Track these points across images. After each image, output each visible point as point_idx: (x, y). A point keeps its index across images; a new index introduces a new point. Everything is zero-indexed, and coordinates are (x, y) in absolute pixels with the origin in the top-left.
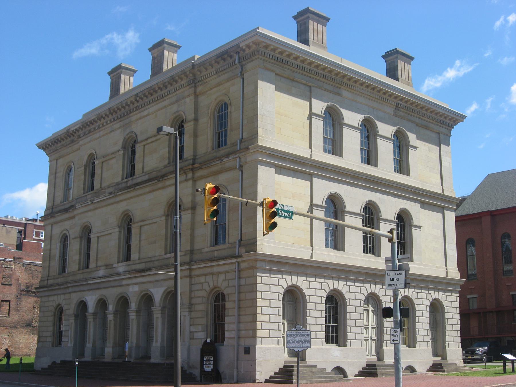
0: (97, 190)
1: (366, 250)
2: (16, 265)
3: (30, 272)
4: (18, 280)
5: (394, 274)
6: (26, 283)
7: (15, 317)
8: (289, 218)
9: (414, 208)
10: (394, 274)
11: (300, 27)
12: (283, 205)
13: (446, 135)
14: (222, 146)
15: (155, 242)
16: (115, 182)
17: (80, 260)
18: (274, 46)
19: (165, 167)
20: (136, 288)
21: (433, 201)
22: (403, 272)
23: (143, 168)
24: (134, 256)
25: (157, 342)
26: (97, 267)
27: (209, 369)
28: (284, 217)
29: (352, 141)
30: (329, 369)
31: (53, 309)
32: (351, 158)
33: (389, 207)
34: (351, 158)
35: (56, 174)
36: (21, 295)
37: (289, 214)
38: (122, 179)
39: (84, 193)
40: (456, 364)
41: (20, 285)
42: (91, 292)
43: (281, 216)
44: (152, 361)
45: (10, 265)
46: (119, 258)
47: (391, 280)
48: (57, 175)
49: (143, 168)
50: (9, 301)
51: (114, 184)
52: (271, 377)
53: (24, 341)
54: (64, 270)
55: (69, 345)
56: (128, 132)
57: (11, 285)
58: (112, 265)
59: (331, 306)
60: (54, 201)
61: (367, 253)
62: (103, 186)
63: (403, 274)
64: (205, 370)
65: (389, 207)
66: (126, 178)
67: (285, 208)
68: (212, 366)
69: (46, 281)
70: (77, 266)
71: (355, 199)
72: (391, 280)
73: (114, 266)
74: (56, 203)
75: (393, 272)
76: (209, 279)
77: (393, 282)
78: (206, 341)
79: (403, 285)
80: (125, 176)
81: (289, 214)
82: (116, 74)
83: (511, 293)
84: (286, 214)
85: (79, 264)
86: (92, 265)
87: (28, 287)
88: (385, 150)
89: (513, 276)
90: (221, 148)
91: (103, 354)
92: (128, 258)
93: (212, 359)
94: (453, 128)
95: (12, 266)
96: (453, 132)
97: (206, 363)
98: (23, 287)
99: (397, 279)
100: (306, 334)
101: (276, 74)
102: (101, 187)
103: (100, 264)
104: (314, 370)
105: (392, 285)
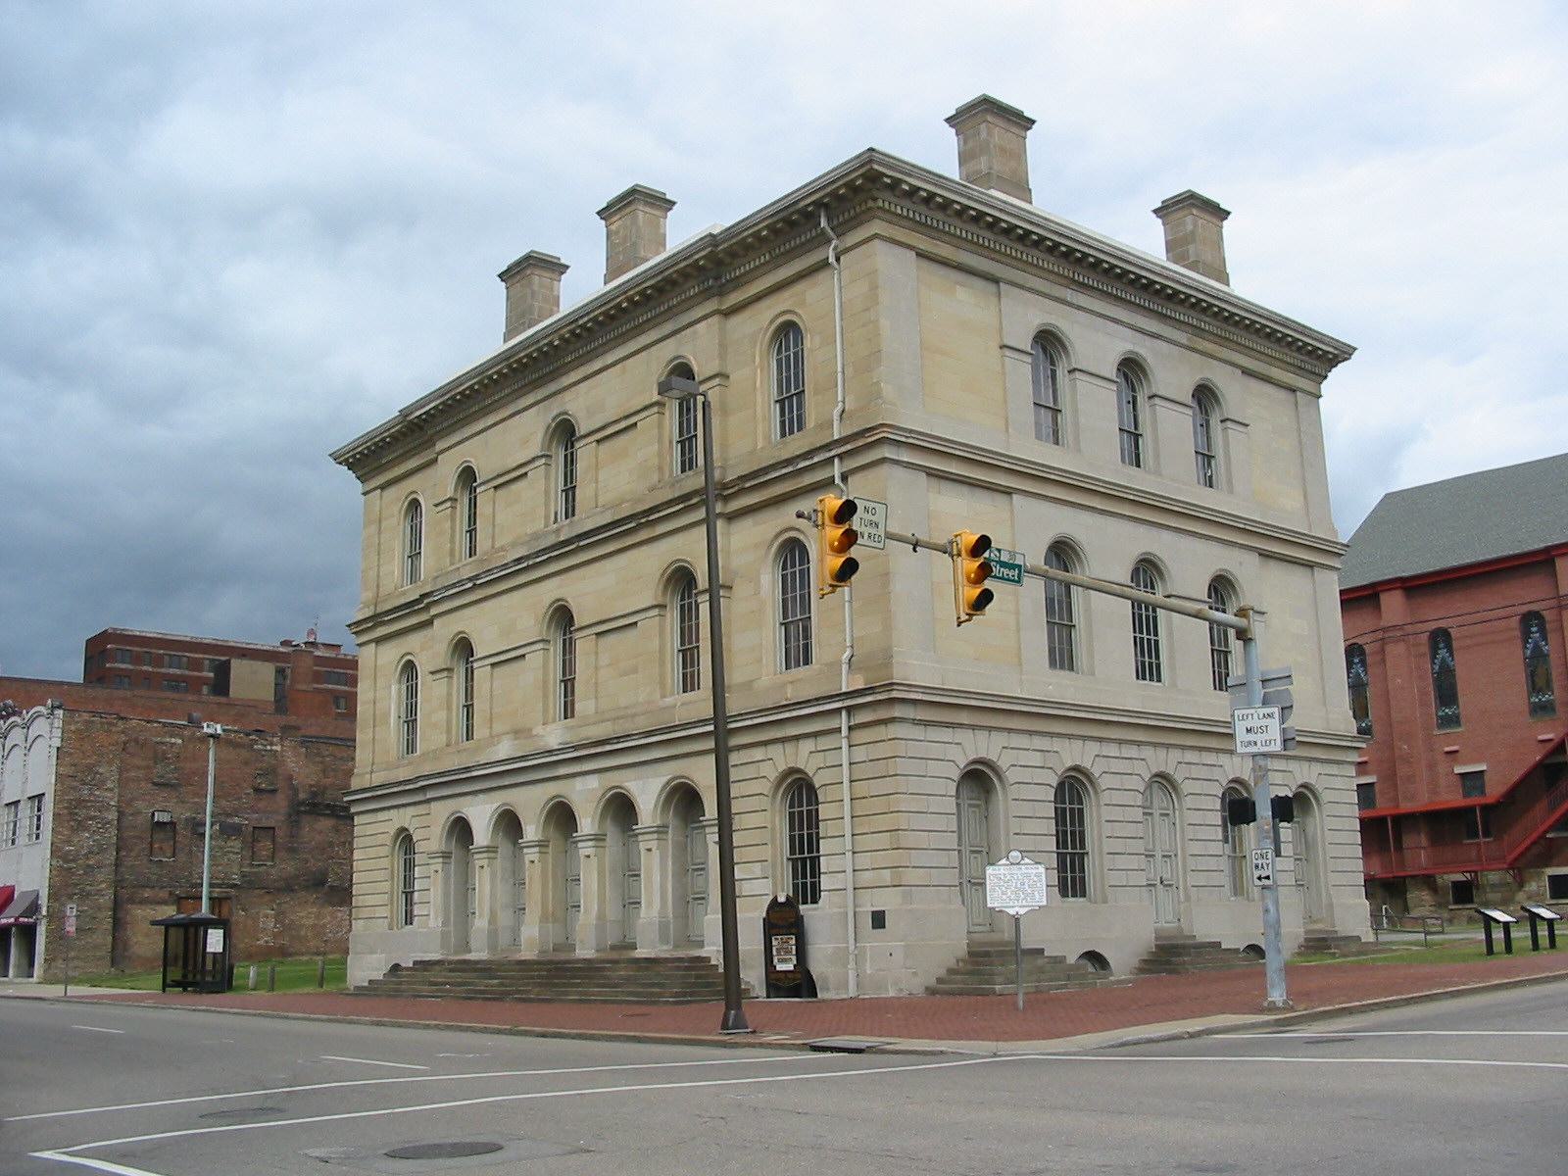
0: (486, 553)
1: (1141, 674)
2: (286, 743)
3: (318, 759)
4: (291, 778)
5: (1255, 716)
6: (311, 786)
7: (287, 867)
8: (1013, 581)
9: (1243, 567)
10: (1255, 716)
11: (965, 142)
12: (999, 550)
13: (1310, 393)
14: (791, 432)
15: (635, 670)
16: (529, 531)
17: (449, 722)
18: (910, 185)
19: (652, 489)
20: (593, 783)
21: (1293, 550)
22: (1276, 710)
23: (596, 496)
24: (583, 706)
25: (650, 904)
26: (491, 736)
27: (790, 967)
28: (1002, 578)
29: (1095, 408)
30: (1072, 959)
31: (388, 839)
32: (1093, 449)
33: (1190, 566)
34: (1093, 449)
35: (380, 522)
36: (298, 813)
37: (1016, 573)
38: (546, 526)
39: (452, 564)
40: (1359, 938)
41: (295, 790)
42: (481, 796)
43: (995, 577)
44: (641, 953)
45: (271, 744)
46: (545, 711)
47: (1249, 731)
48: (384, 525)
49: (596, 496)
50: (274, 828)
51: (527, 539)
52: (940, 980)
53: (311, 922)
54: (411, 747)
55: (432, 923)
56: (555, 413)
57: (274, 791)
58: (530, 730)
59: (1068, 806)
60: (378, 586)
61: (1144, 679)
62: (497, 545)
63: (1276, 715)
64: (778, 968)
65: (1190, 566)
66: (556, 521)
67: (1004, 558)
68: (794, 958)
69: (368, 776)
70: (444, 738)
71: (1110, 547)
72: (1249, 731)
73: (534, 733)
74: (383, 591)
75: (1253, 711)
76: (775, 751)
77: (1251, 737)
78: (776, 898)
79: (1279, 742)
80: (552, 518)
81: (1016, 573)
82: (530, 272)
83: (1458, 770)
84: (1006, 571)
85: (449, 731)
86: (479, 732)
87: (314, 795)
88: (1171, 428)
89: (1460, 730)
90: (789, 438)
91: (515, 941)
92: (569, 711)
93: (794, 942)
94: (1326, 377)
95: (274, 748)
96: (1326, 387)
97: (779, 953)
98: (302, 796)
99: (1263, 729)
100: (1034, 871)
101: (918, 254)
102: (493, 547)
103: (498, 728)
104: (1040, 962)
105: (1249, 743)
